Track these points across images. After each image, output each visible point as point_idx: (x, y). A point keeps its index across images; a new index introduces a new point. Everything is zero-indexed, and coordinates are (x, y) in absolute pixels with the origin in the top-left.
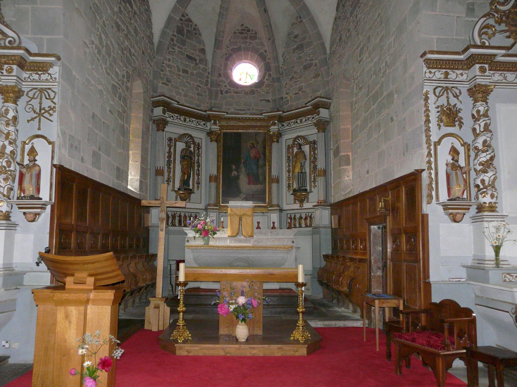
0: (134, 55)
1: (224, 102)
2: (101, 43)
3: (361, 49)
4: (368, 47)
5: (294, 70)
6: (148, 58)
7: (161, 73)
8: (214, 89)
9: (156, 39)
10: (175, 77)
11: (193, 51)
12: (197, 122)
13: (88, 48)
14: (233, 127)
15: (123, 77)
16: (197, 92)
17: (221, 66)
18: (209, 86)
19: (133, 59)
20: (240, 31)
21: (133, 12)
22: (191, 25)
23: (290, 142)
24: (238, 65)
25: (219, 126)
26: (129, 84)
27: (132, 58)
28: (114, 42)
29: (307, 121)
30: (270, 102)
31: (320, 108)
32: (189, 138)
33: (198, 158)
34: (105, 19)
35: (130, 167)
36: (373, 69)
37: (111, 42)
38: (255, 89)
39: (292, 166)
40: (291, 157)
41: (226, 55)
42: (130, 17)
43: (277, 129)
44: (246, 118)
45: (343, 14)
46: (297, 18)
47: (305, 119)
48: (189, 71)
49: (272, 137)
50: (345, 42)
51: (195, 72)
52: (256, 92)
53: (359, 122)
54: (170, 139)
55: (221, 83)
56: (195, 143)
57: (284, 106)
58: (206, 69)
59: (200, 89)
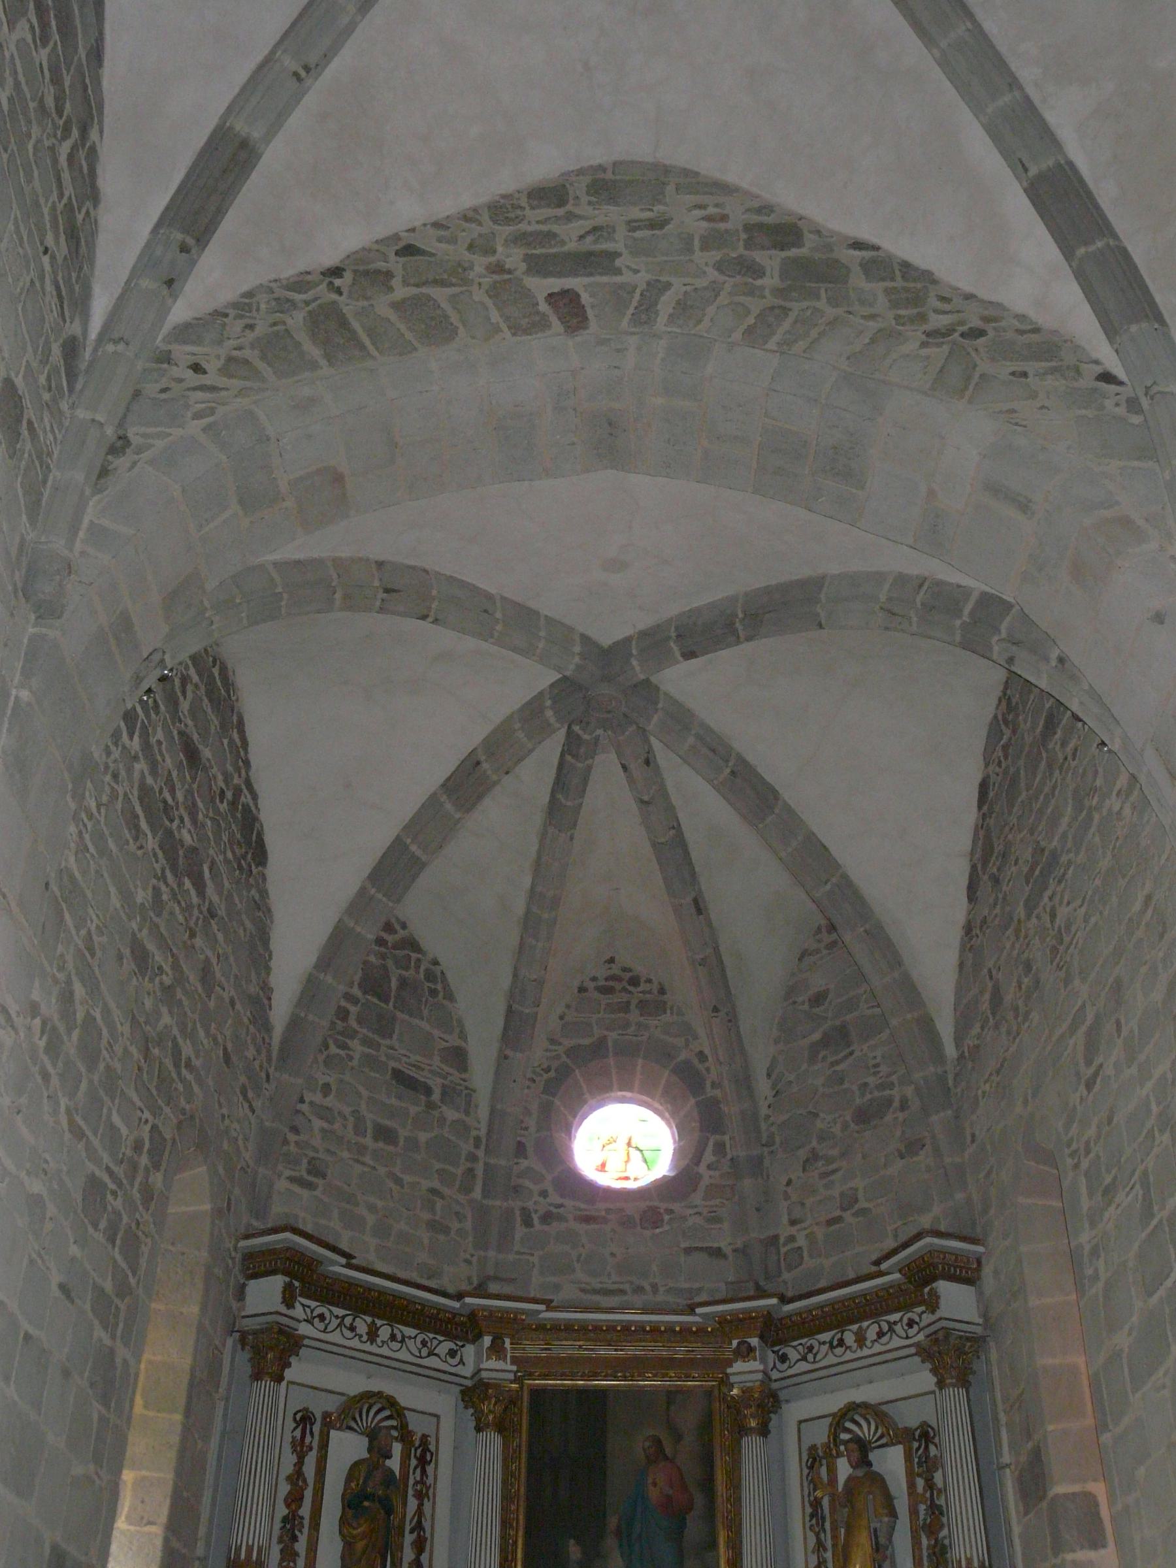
0: (188, 1065)
1: (535, 1259)
2: (67, 1013)
3: (1089, 1034)
4: (1118, 1023)
5: (819, 1124)
6: (243, 1079)
7: (292, 1137)
8: (498, 1203)
9: (280, 1012)
10: (345, 1154)
11: (418, 1058)
12: (424, 1343)
13: (12, 1027)
14: (570, 1366)
15: (138, 1147)
16: (426, 1216)
17: (527, 1112)
18: (477, 1194)
19: (182, 1080)
20: (602, 983)
21: (205, 909)
22: (419, 960)
23: (819, 1435)
24: (593, 1109)
25: (514, 1360)
26: (157, 1179)
27: (179, 1074)
28: (117, 1014)
29: (885, 1339)
30: (725, 1256)
31: (934, 1279)
32: (387, 1413)
33: (421, 1505)
34: (93, 928)
35: (114, 1548)
36: (1154, 1108)
37: (106, 1011)
38: (663, 1206)
39: (834, 1546)
40: (826, 1503)
41: (548, 1070)
42: (192, 924)
43: (760, 1376)
44: (626, 1327)
45: (997, 910)
46: (819, 930)
47: (875, 1328)
48: (403, 1133)
49: (738, 1412)
50: (1016, 1009)
51: (423, 1137)
52: (666, 1217)
53: (1123, 1340)
54: (304, 1419)
55: (527, 1183)
56: (410, 1434)
57: (786, 1276)
58: (467, 1129)
59: (439, 1204)
